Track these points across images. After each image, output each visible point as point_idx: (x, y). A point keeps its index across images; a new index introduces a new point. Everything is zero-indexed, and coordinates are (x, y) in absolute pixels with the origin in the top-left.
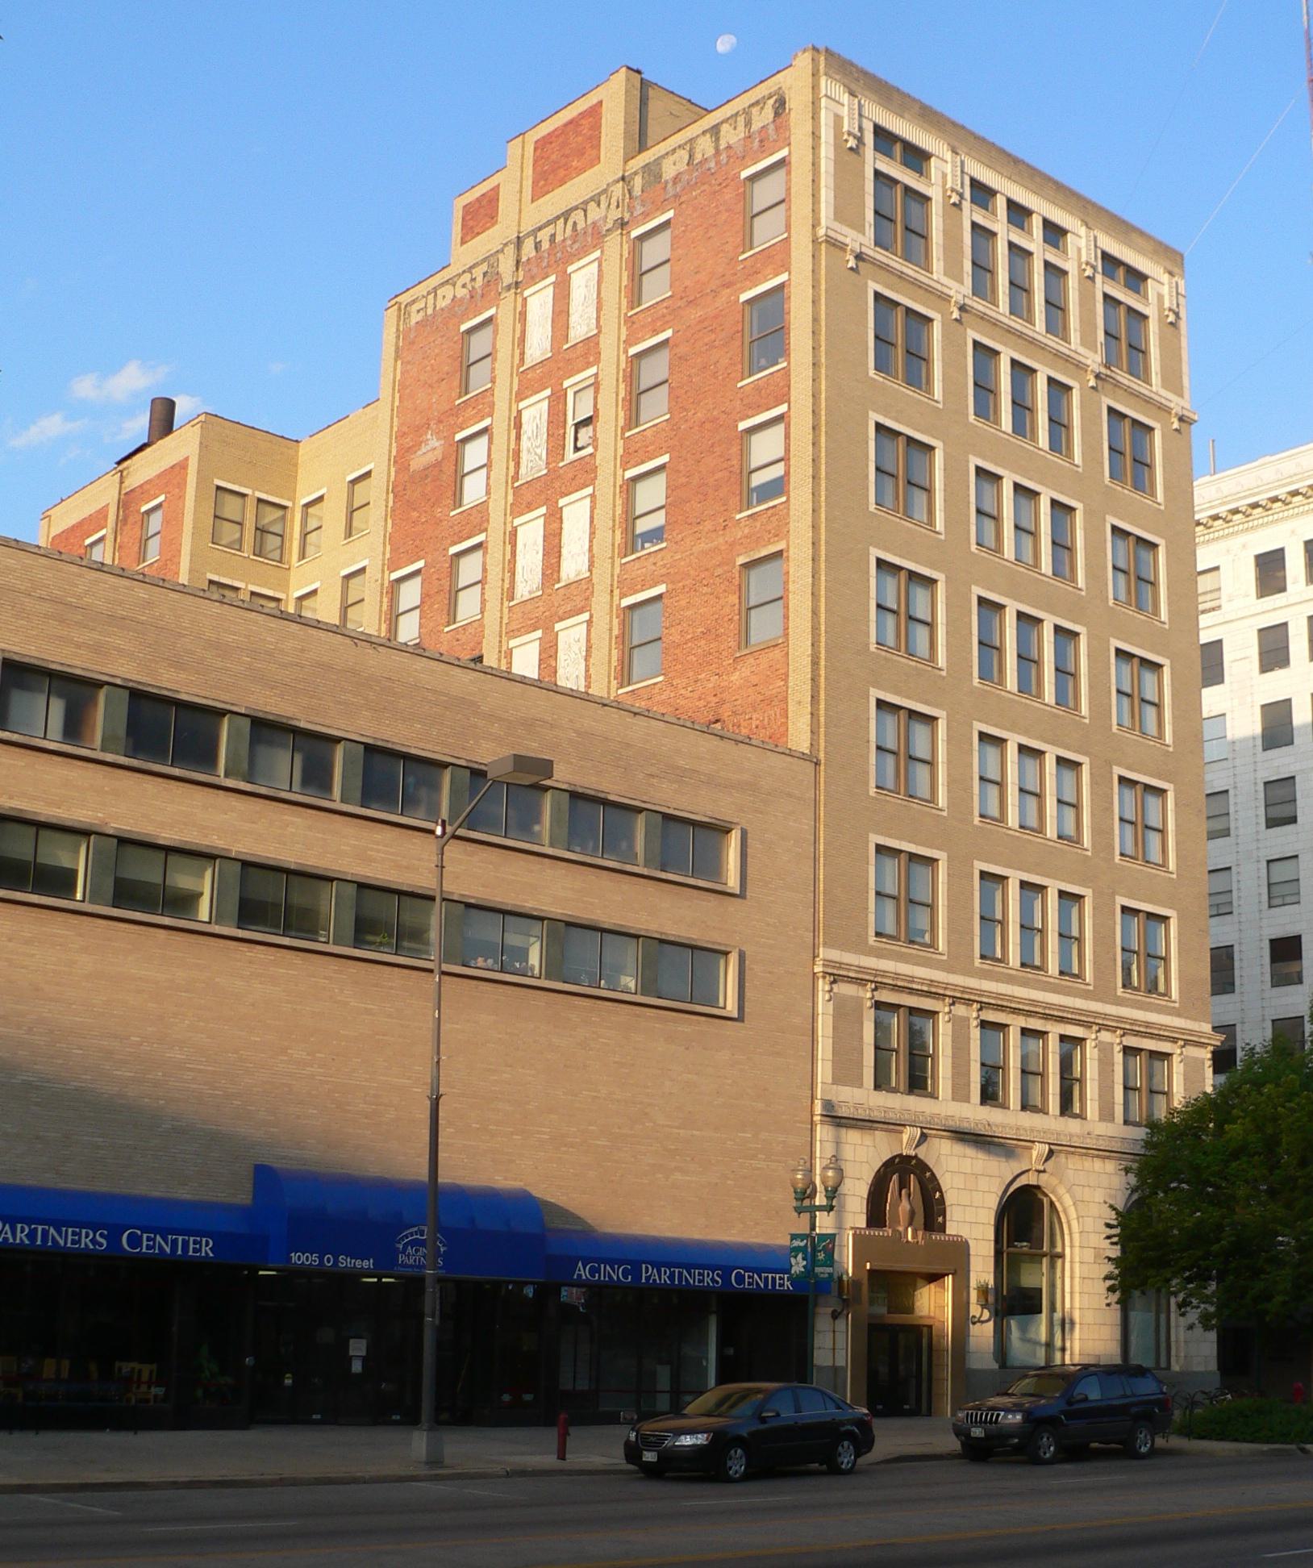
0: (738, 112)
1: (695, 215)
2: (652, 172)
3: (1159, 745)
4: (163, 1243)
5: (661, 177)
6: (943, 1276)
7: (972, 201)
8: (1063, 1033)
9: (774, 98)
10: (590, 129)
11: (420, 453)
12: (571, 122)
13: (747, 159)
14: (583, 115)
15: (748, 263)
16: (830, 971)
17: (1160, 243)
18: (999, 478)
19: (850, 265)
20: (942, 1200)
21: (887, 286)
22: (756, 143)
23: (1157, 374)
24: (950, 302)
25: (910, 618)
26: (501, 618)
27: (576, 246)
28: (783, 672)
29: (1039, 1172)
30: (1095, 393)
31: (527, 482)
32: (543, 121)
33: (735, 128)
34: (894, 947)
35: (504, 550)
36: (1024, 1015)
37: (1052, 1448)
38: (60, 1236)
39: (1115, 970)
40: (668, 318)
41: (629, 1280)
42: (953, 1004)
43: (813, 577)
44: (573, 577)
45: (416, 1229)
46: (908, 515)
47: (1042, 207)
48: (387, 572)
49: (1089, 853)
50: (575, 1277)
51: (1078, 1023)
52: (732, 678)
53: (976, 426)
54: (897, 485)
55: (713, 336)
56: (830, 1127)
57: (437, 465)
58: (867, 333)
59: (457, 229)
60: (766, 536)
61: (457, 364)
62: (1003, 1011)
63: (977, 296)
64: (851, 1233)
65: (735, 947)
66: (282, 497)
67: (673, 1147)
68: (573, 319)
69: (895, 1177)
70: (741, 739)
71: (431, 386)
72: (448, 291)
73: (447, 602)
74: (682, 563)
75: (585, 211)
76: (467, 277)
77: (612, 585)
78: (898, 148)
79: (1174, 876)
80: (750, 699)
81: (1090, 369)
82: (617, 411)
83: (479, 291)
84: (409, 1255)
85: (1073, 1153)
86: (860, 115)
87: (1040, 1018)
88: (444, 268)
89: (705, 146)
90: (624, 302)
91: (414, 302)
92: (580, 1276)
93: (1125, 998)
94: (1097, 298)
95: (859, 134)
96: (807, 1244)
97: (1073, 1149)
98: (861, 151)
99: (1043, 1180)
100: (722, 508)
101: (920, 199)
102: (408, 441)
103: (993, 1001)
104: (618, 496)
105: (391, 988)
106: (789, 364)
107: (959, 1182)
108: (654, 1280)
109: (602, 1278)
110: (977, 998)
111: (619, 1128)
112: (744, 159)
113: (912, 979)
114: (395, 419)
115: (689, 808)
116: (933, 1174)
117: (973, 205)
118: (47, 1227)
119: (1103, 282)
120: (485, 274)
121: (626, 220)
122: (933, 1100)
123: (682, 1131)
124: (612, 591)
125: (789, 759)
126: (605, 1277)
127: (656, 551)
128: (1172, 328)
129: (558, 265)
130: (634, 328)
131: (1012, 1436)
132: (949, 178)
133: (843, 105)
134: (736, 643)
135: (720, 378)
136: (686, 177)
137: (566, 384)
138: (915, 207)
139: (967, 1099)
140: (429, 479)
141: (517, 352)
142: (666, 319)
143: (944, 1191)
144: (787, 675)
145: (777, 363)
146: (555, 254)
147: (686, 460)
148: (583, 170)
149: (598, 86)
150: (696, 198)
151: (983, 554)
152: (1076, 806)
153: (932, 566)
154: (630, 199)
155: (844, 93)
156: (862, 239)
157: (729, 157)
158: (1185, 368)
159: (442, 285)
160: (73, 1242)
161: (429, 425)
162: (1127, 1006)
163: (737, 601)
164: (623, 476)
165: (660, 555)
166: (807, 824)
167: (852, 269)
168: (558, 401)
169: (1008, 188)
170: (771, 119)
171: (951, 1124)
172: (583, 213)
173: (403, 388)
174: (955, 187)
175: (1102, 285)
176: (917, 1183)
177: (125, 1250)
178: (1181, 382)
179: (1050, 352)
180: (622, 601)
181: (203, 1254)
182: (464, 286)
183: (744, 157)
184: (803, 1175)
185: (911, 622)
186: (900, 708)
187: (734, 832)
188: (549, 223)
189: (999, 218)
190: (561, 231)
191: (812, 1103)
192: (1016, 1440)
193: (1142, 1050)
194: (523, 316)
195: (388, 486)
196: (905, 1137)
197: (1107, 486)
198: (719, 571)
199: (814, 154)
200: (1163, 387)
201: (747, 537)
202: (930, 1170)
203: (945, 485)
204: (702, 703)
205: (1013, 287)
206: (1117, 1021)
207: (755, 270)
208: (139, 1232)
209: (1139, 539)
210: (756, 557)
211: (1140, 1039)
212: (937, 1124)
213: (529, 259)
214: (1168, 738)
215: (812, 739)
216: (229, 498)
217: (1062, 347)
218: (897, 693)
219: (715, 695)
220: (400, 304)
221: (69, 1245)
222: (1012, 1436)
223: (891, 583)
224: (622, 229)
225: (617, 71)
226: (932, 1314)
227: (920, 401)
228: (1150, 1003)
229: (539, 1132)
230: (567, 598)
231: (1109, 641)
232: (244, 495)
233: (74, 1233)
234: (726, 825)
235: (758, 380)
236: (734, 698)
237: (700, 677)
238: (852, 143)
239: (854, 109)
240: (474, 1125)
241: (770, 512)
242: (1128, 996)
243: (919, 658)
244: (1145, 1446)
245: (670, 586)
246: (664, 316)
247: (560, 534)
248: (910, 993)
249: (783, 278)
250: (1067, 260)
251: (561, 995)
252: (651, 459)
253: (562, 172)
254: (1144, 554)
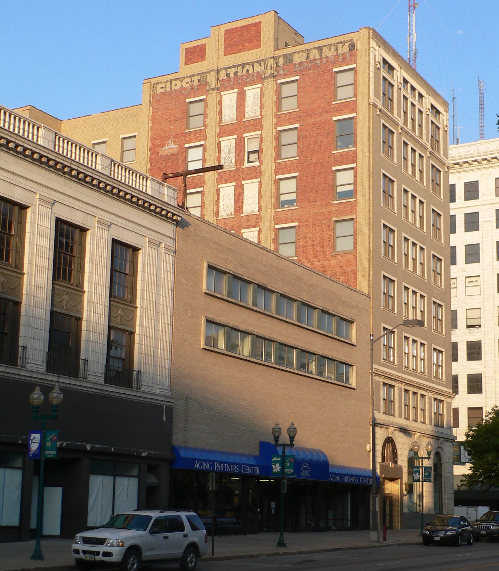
0: (331, 44)
1: (310, 81)
2: (288, 58)
5: (293, 61)
6: (397, 479)
9: (349, 43)
11: (164, 148)
12: (245, 26)
22: (340, 59)
24: (398, 126)
27: (248, 80)
28: (355, 263)
32: (229, 22)
33: (330, 50)
40: (297, 119)
55: (320, 131)
60: (346, 212)
68: (247, 109)
71: (170, 121)
72: (179, 84)
74: (305, 216)
75: (253, 66)
77: (271, 219)
79: (444, 337)
83: (196, 87)
85: (423, 436)
89: (315, 54)
90: (275, 108)
100: (325, 198)
102: (158, 142)
104: (273, 185)
106: (356, 148)
116: (395, 444)
120: (199, 80)
122: (393, 417)
127: (293, 209)
129: (239, 85)
130: (280, 119)
131: (496, 533)
132: (399, 78)
140: (171, 160)
142: (296, 119)
144: (356, 264)
145: (348, 147)
146: (237, 81)
148: (250, 49)
157: (327, 61)
161: (169, 138)
165: (295, 211)
172: (252, 67)
180: (276, 226)
183: (334, 63)
187: (354, 323)
194: (220, 102)
196: (390, 431)
198: (324, 221)
200: (443, 155)
201: (337, 211)
202: (394, 442)
207: (340, 109)
210: (342, 219)
213: (223, 79)
222: (496, 533)
225: (270, 12)
226: (392, 493)
237: (315, 260)
241: (348, 203)
245: (300, 224)
247: (243, 195)
248: (390, 380)
249: (354, 115)
253: (240, 47)
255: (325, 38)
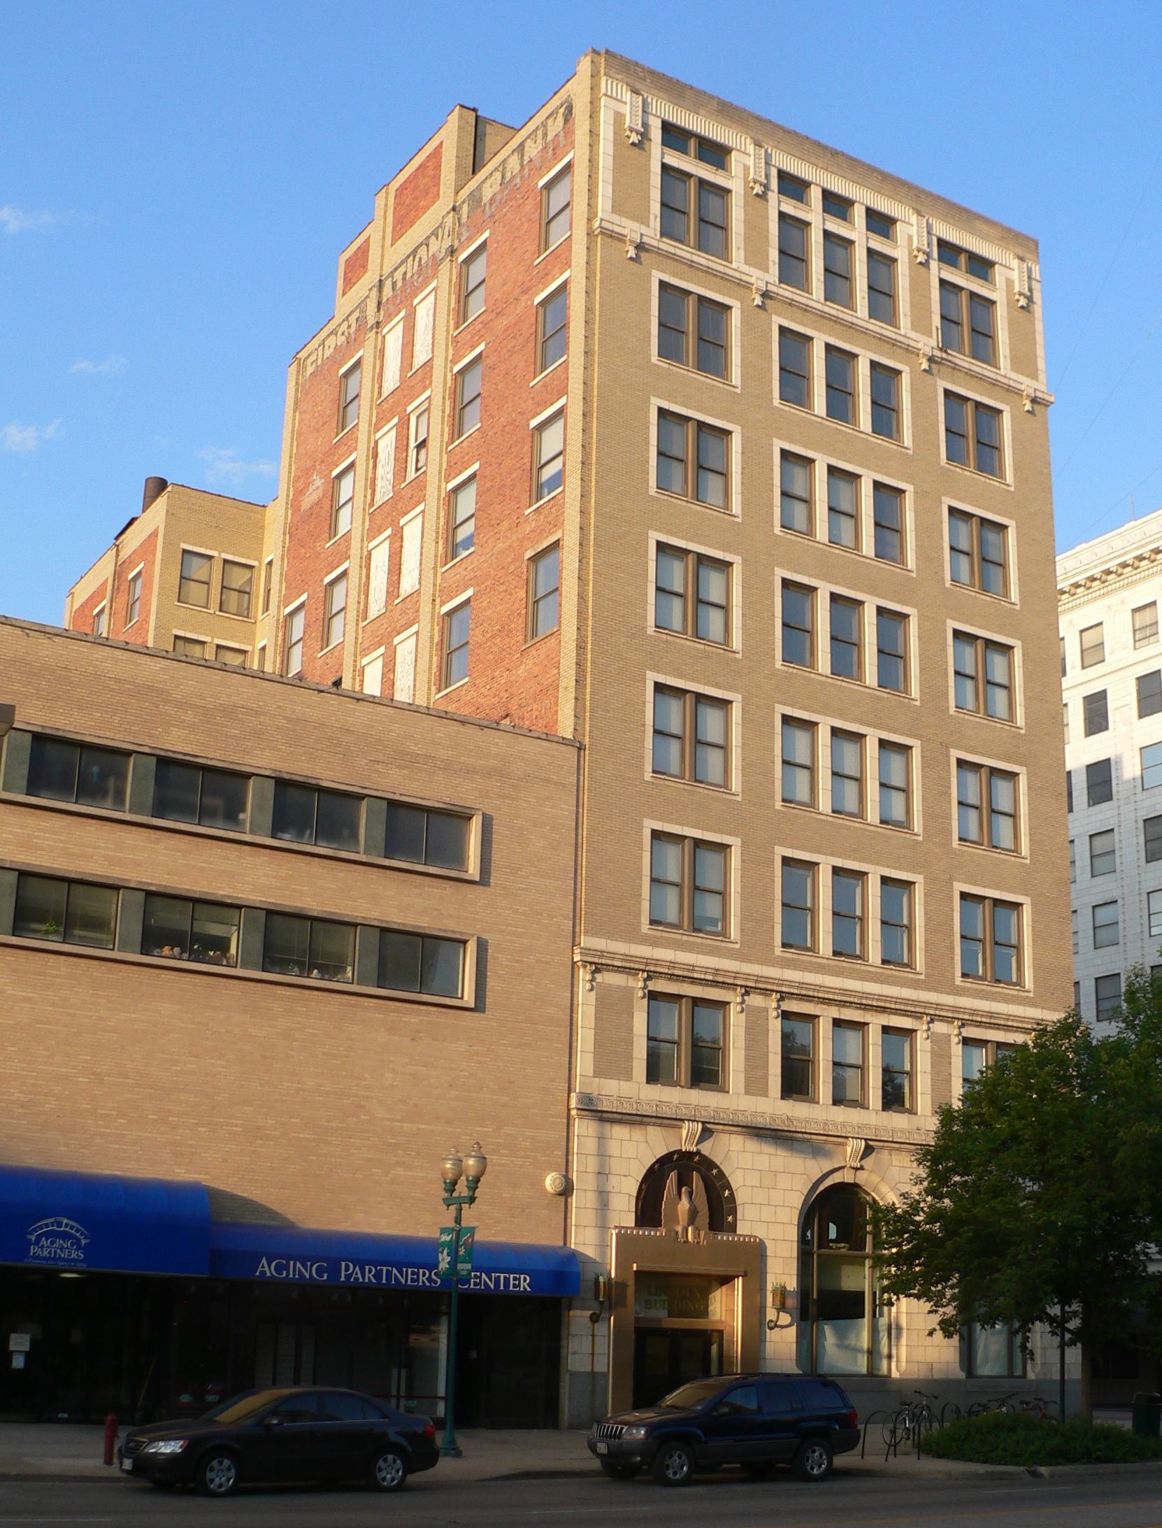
0: (537, 127)
2: (475, 197)
3: (1008, 728)
4: (399, 1276)
5: (481, 201)
7: (940, 259)
8: (886, 1024)
10: (433, 170)
13: (543, 168)
14: (429, 158)
15: (541, 267)
16: (590, 959)
17: (1010, 230)
18: (810, 461)
19: (923, 367)
20: (732, 1198)
21: (953, 383)
22: (550, 152)
23: (1005, 357)
25: (989, 682)
26: (356, 638)
27: (420, 279)
29: (857, 1169)
30: (928, 377)
31: (379, 507)
34: (675, 936)
35: (360, 574)
36: (837, 1005)
37: (685, 1469)
38: (306, 1270)
39: (953, 959)
41: (325, 1278)
42: (932, 1021)
43: (580, 561)
44: (409, 591)
45: (52, 1220)
46: (698, 497)
47: (863, 197)
48: (282, 608)
49: (920, 838)
50: (258, 1274)
51: (905, 1013)
52: (519, 672)
53: (783, 410)
54: (686, 469)
55: (514, 342)
56: (591, 1122)
57: (319, 503)
58: (650, 321)
59: (340, 283)
61: (336, 406)
62: (811, 1001)
63: (832, 301)
64: (614, 1232)
65: (473, 935)
66: (248, 558)
67: (393, 1141)
69: (673, 1175)
70: (486, 723)
72: (331, 342)
73: (321, 629)
74: (485, 565)
75: (427, 245)
76: (345, 325)
77: (434, 595)
78: (963, 259)
79: (1028, 862)
80: (531, 690)
81: (1025, 393)
82: (442, 428)
84: (42, 1247)
85: (898, 1149)
86: (1030, 278)
87: (857, 1008)
88: (330, 321)
91: (309, 355)
92: (263, 1273)
93: (965, 988)
94: (932, 284)
95: (1029, 294)
96: (452, 1238)
97: (897, 1146)
98: (646, 147)
99: (862, 1178)
101: (886, 261)
102: (300, 484)
103: (795, 991)
105: (56, 976)
107: (753, 1179)
108: (357, 1279)
109: (291, 1276)
110: (775, 988)
111: (329, 1121)
112: (540, 171)
113: (693, 968)
114: (293, 465)
115: (420, 794)
116: (721, 1172)
117: (780, 196)
118: (390, 1268)
119: (940, 269)
121: (455, 247)
123: (405, 1125)
124: (434, 600)
125: (546, 744)
126: (294, 1275)
128: (1023, 313)
133: (750, 155)
134: (523, 637)
135: (518, 381)
136: (499, 197)
137: (409, 409)
138: (713, 201)
139: (764, 1093)
141: (376, 387)
143: (734, 1189)
147: (491, 465)
149: (440, 128)
150: (506, 215)
151: (789, 536)
152: (906, 791)
153: (725, 549)
154: (459, 226)
155: (913, 214)
156: (651, 231)
157: (530, 170)
158: (1040, 351)
159: (329, 336)
160: (412, 1280)
162: (968, 996)
163: (524, 595)
164: (446, 489)
166: (567, 809)
167: (1028, 411)
168: (404, 425)
169: (821, 178)
170: (562, 127)
171: (742, 1120)
173: (299, 437)
174: (1022, 291)
175: (937, 271)
176: (701, 1183)
177: (316, 1279)
178: (1036, 364)
179: (874, 337)
181: (522, 1289)
182: (343, 334)
183: (541, 168)
184: (453, 1164)
185: (989, 686)
186: (685, 692)
187: (474, 817)
188: (400, 265)
189: (813, 208)
190: (411, 268)
191: (569, 1096)
192: (639, 1459)
193: (988, 1041)
195: (285, 528)
197: (943, 467)
198: (512, 568)
199: (591, 151)
202: (717, 1167)
203: (743, 468)
204: (497, 699)
205: (872, 292)
206: (953, 1012)
208: (284, 1262)
209: (983, 521)
210: (540, 549)
211: (983, 1030)
212: (723, 1119)
214: (1020, 719)
215: (576, 724)
216: (196, 560)
217: (888, 331)
218: (681, 676)
219: (506, 691)
220: (300, 359)
221: (409, 1283)
223: (968, 651)
224: (452, 256)
226: (723, 1319)
227: (714, 386)
228: (996, 993)
229: (228, 1125)
230: (404, 612)
231: (945, 621)
232: (210, 558)
233: (413, 1273)
234: (468, 811)
235: (545, 377)
236: (520, 692)
238: (1023, 302)
239: (1023, 272)
240: (151, 1117)
241: (552, 503)
242: (969, 985)
243: (999, 719)
244: (820, 1466)
246: (479, 331)
248: (692, 983)
250: (896, 247)
251: (259, 985)
252: (466, 469)
254: (992, 536)
255: (527, 119)
